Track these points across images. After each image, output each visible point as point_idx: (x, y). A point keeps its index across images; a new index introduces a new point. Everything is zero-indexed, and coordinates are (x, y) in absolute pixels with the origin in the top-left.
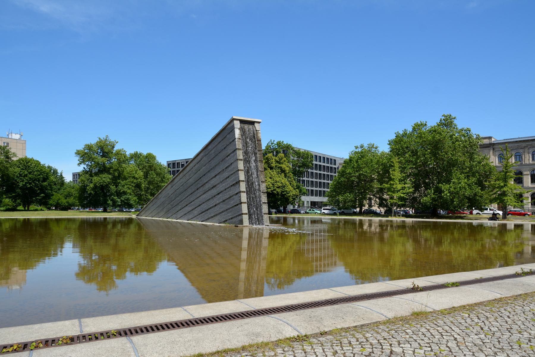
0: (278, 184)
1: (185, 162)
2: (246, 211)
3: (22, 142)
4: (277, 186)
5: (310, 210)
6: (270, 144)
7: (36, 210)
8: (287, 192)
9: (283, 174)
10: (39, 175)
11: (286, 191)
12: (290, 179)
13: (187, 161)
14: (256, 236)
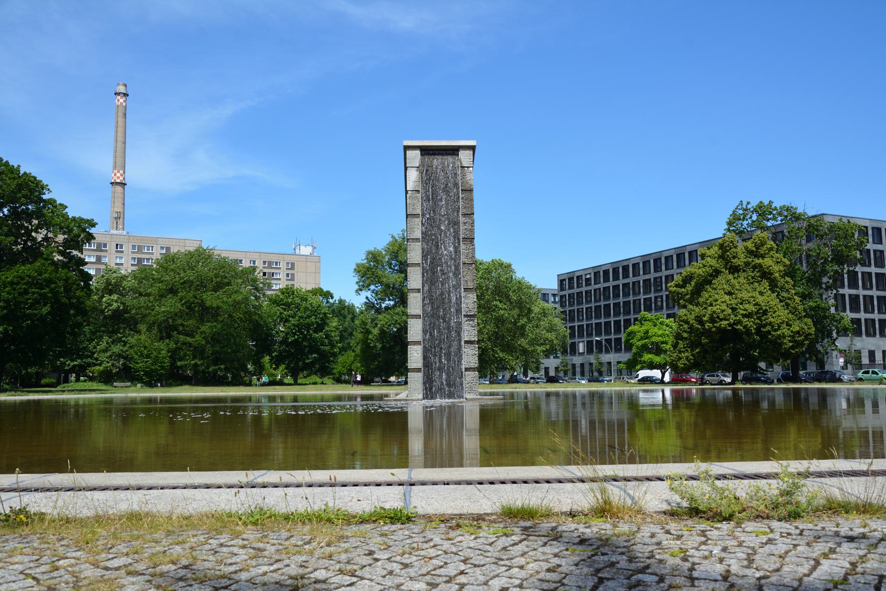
0: (747, 306)
1: (593, 274)
2: (419, 365)
3: (314, 260)
4: (744, 312)
5: (867, 372)
6: (741, 212)
7: (315, 383)
8: (773, 326)
9: (766, 283)
10: (309, 317)
11: (770, 324)
12: (785, 294)
13: (596, 271)
14: (445, 422)
